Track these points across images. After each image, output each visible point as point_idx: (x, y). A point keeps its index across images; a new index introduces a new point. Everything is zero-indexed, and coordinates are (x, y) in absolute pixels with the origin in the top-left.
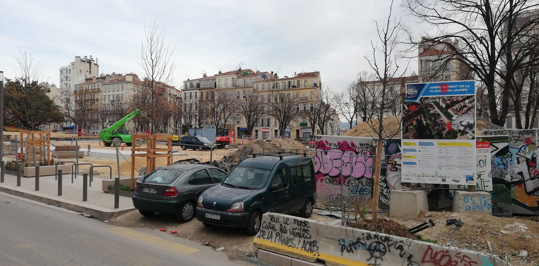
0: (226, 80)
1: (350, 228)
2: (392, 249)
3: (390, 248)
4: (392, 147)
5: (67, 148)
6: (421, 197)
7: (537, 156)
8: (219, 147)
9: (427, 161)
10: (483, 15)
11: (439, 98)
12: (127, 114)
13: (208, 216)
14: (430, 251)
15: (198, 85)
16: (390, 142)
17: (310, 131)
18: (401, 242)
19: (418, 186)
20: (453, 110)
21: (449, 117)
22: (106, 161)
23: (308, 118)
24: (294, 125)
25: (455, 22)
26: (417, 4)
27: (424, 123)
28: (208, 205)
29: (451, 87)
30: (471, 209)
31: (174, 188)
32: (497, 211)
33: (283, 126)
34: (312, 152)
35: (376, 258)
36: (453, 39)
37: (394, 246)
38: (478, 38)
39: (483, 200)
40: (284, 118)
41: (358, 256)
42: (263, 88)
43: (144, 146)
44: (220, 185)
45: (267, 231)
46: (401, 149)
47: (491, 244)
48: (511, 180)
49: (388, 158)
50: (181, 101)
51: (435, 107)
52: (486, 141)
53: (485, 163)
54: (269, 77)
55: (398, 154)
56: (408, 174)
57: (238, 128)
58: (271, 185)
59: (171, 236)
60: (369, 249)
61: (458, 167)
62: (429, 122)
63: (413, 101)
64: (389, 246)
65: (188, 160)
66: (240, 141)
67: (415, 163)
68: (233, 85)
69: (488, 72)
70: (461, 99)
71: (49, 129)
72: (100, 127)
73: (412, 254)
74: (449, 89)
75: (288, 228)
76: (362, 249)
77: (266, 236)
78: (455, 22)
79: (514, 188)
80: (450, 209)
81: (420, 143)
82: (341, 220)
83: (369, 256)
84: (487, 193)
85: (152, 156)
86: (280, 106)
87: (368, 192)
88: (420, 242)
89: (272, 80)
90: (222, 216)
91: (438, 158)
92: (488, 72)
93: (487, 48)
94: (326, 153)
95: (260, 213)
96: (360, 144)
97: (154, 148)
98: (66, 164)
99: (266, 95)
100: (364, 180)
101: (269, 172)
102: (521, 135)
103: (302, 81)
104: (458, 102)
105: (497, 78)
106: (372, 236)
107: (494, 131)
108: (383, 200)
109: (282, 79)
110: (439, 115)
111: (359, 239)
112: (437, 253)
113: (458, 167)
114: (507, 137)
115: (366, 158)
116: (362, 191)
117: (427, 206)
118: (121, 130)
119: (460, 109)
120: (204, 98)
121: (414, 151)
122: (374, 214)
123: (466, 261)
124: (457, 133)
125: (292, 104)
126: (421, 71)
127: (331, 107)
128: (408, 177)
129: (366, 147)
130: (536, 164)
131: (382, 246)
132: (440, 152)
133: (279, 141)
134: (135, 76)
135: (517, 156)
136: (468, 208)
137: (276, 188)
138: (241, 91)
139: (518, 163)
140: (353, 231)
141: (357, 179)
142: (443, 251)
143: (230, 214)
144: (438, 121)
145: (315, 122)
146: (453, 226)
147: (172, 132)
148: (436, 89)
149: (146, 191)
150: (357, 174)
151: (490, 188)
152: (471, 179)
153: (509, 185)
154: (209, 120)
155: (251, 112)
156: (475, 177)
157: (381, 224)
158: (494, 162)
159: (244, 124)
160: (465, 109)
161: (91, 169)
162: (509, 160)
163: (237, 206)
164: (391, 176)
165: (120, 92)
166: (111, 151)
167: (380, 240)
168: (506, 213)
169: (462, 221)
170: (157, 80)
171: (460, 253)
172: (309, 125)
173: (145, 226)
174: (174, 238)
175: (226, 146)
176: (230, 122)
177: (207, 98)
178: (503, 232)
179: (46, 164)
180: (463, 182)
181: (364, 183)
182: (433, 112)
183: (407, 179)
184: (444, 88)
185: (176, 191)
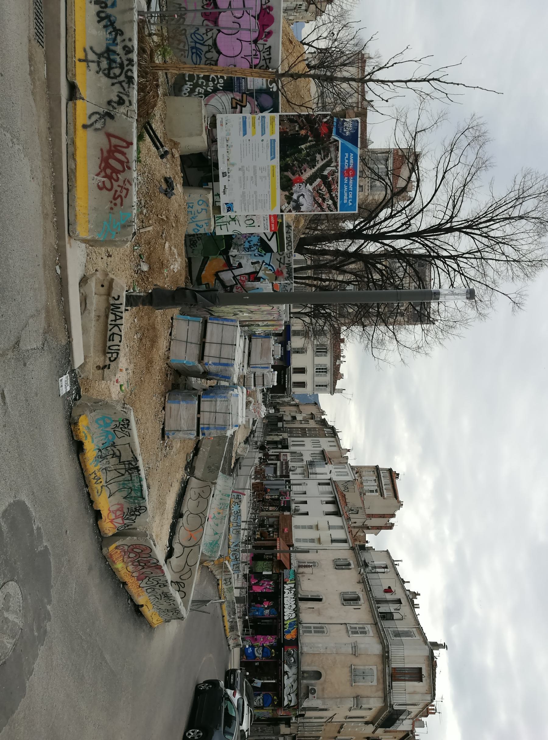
3: (118, 86)
4: (266, 101)
6: (199, 143)
7: (262, 283)
9: (248, 150)
10: (440, 224)
11: (336, 166)
14: (124, 144)
16: (274, 96)
18: (130, 103)
19: (213, 140)
20: (319, 185)
21: (311, 180)
25: (436, 191)
26: (471, 139)
27: (303, 147)
29: (351, 182)
30: (190, 209)
32: (191, 241)
36: (412, 194)
37: (122, 91)
38: (409, 220)
39: (203, 223)
41: (94, 32)
47: (149, 231)
48: (232, 256)
49: (251, 94)
51: (324, 161)
53: (250, 226)
55: (257, 110)
56: (230, 124)
61: (244, 193)
62: (304, 152)
63: (334, 130)
64: (120, 83)
67: (245, 133)
69: (365, 232)
70: (334, 195)
73: (116, 119)
74: (349, 179)
76: (107, 39)
78: (436, 191)
79: (221, 259)
80: (187, 184)
81: (275, 140)
82: (146, 10)
83: (98, 51)
84: (212, 228)
91: (255, 167)
92: (365, 232)
93: (395, 231)
96: (270, 47)
100: (214, 54)
102: (286, 265)
104: (330, 191)
105: (243, 525)
106: (130, 56)
107: (292, 237)
110: (314, 166)
111: (122, 34)
112: (124, 154)
113: (244, 193)
114: (284, 250)
115: (249, 58)
119: (320, 193)
121: (263, 133)
123: (121, 192)
124: (289, 191)
126: (374, 152)
128: (224, 124)
129: (267, 57)
130: (252, 281)
131: (117, 71)
135: (261, 261)
136: (191, 205)
139: (253, 263)
142: (128, 162)
144: (305, 165)
146: (164, 186)
148: (349, 163)
150: (223, 42)
151: (219, 232)
152: (229, 209)
153: (225, 253)
156: (232, 214)
158: (252, 237)
160: (320, 201)
162: (256, 252)
164: (224, 99)
167: (126, 68)
168: (190, 250)
169: (173, 197)
171: (131, 185)
178: (167, 245)
180: (224, 200)
181: (209, 55)
182: (317, 159)
183: (222, 122)
184: (350, 173)
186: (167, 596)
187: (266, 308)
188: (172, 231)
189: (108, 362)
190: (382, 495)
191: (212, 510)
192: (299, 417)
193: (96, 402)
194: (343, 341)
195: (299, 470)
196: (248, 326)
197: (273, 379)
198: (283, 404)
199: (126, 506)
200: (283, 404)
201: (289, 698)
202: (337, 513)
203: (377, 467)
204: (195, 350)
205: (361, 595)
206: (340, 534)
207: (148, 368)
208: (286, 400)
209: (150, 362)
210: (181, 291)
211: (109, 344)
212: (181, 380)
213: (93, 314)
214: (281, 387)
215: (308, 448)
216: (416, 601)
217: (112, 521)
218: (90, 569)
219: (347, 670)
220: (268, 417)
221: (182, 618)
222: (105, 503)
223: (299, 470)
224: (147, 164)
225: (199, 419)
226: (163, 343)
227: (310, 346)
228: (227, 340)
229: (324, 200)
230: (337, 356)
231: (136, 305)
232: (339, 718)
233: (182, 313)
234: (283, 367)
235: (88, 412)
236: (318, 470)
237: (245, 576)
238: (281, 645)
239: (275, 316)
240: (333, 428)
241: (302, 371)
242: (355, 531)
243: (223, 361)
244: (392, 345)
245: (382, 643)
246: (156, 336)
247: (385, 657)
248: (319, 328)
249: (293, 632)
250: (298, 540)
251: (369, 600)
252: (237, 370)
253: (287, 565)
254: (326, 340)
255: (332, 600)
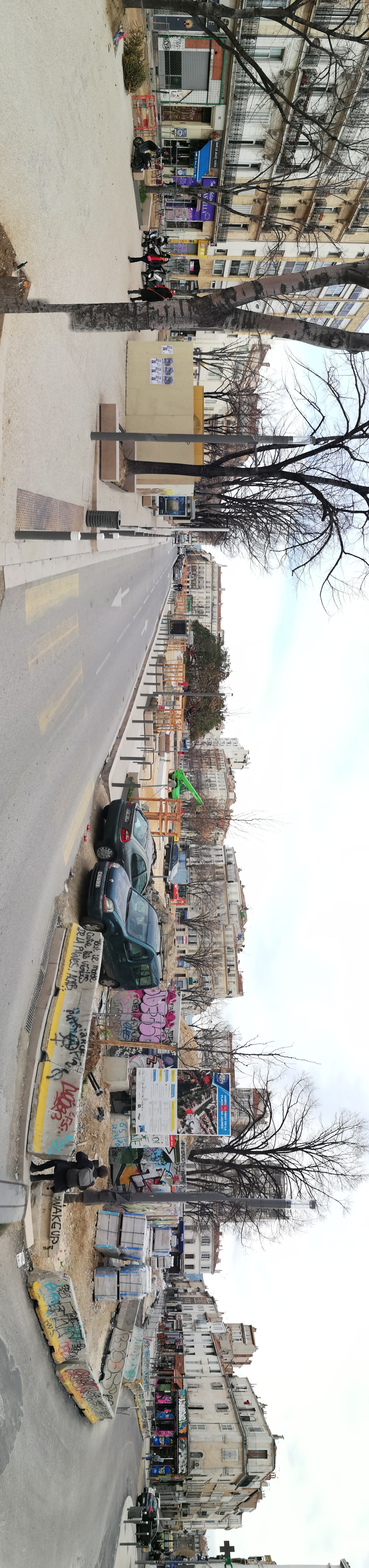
0: (236, 893)
1: (90, 1018)
2: (73, 1055)
4: (170, 1061)
5: (167, 743)
8: (167, 887)
9: (157, 1091)
12: (198, 792)
13: (100, 874)
15: (230, 863)
16: (175, 1058)
17: (185, 988)
19: (133, 1083)
21: (198, 1112)
22: (155, 775)
23: (197, 985)
24: (191, 972)
28: (111, 874)
31: (129, 839)
33: (190, 959)
34: (164, 986)
35: (63, 1042)
39: (122, 1139)
40: (197, 960)
41: (63, 1025)
42: (228, 936)
43: (169, 811)
44: (130, 886)
45: (85, 937)
46: (168, 1068)
49: (160, 1057)
50: (212, 845)
52: (176, 1144)
53: (156, 1142)
54: (239, 942)
56: (145, 1075)
57: (186, 909)
58: (131, 942)
59: (82, 836)
60: (70, 1035)
65: (155, 852)
66: (174, 911)
68: (231, 902)
71: (183, 730)
72: (186, 770)
75: (89, 960)
77: (79, 936)
80: (113, 1111)
85: (160, 817)
86: (209, 955)
87: (127, 1038)
88: (81, 1081)
89: (236, 946)
90: (100, 888)
94: (163, 1000)
95: (103, 931)
97: (168, 819)
98: (154, 743)
99: (221, 939)
100: (138, 1034)
101: (144, 940)
103: (234, 979)
104: (211, 1120)
107: (185, 1151)
108: (120, 1050)
109: (236, 957)
112: (72, 1095)
116: (127, 1033)
117: (115, 1090)
118: (184, 788)
120: (217, 870)
121: (167, 1080)
122: (105, 1042)
125: (212, 968)
127: (208, 1008)
131: (74, 1046)
132: (165, 1103)
133: (174, 955)
134: (234, 801)
137: (127, 948)
138: (225, 910)
140: (88, 1021)
141: (138, 1029)
143: (101, 897)
145: (193, 992)
146: (97, 1113)
147: (182, 834)
149: (128, 812)
150: (143, 1028)
151: (134, 1146)
152: (142, 1130)
153: (138, 1162)
154: (194, 877)
155: (204, 922)
157: (95, 1047)
159: (190, 915)
161: (149, 763)
162: (160, 1162)
163: (109, 905)
164: (143, 1059)
165: (218, 788)
166: (165, 780)
170: (231, 822)
172: (190, 986)
173: (93, 810)
174: (80, 840)
175: (168, 895)
176: (193, 900)
177: (217, 873)
179: (155, 728)
180: (138, 1123)
184: (225, 1108)
185: (125, 840)
186: (101, 1403)
187: (165, 1205)
188: (101, 1145)
189: (51, 1244)
190: (244, 1342)
191: (130, 1350)
192: (189, 1290)
193: (45, 1272)
194: (221, 1234)
195: (189, 1326)
196: (153, 1220)
197: (170, 1262)
198: (178, 1281)
199: (71, 1343)
200: (178, 1281)
201: (182, 1469)
202: (214, 1354)
203: (242, 1325)
204: (114, 1238)
205: (230, 1406)
206: (216, 1367)
207: (80, 1250)
208: (180, 1278)
209: (82, 1246)
210: (105, 1192)
211: (52, 1230)
212: (104, 1260)
213: (40, 1208)
214: (176, 1269)
215: (195, 1311)
216: (265, 1410)
217: (61, 1354)
218: (48, 1385)
219: (219, 1452)
220: (167, 1290)
221: (111, 1418)
222: (56, 1341)
223: (189, 1326)
224: (86, 1098)
225: (118, 1288)
226: (90, 1232)
227: (197, 1238)
228: (137, 1230)
229: (207, 1126)
230: (217, 1245)
231: (72, 1202)
232: (213, 1481)
233: (105, 1209)
234: (178, 1253)
235: (39, 1280)
236: (202, 1326)
237: (153, 1393)
238: (176, 1436)
239: (173, 1212)
240: (212, 1298)
241: (191, 1256)
242: (225, 1365)
243: (135, 1246)
244: (255, 1236)
245: (242, 1435)
246: (85, 1226)
247: (244, 1444)
248: (204, 1223)
249: (184, 1429)
250: (188, 1371)
251: (234, 1408)
252: (145, 1253)
253: (180, 1386)
254: (209, 1233)
255: (210, 1408)
